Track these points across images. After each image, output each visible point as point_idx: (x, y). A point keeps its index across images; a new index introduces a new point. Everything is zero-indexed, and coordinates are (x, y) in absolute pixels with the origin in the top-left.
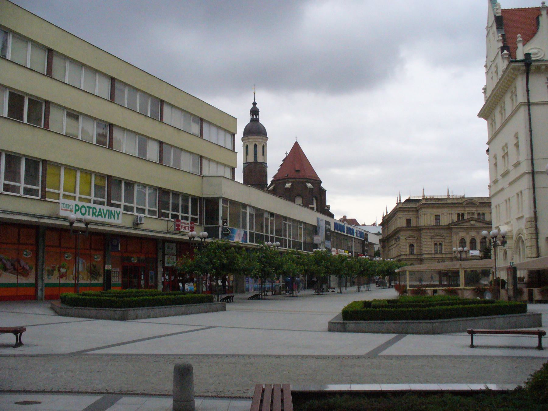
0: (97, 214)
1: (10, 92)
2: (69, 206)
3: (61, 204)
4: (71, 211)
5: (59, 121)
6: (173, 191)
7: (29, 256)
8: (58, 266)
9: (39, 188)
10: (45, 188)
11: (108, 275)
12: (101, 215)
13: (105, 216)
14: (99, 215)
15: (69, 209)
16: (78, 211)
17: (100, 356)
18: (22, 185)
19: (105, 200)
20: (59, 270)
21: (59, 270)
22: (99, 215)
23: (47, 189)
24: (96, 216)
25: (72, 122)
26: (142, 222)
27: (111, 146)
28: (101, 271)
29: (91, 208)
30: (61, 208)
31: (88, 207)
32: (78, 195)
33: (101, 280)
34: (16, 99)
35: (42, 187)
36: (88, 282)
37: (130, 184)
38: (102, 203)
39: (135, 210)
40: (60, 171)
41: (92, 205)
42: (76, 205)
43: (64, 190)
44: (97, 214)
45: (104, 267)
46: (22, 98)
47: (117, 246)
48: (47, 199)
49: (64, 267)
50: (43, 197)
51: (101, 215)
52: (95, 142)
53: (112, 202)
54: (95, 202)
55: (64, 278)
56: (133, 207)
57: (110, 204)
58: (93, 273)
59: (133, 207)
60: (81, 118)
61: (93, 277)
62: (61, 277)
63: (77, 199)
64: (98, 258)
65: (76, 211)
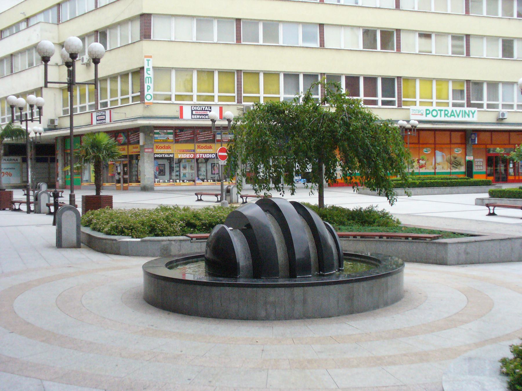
0: (449, 115)
1: (263, 23)
2: (419, 111)
3: (411, 110)
4: (422, 115)
5: (410, 43)
6: (130, 70)
7: (460, 152)
8: (417, 159)
9: (396, 99)
10: (470, 101)
11: (469, 165)
12: (454, 115)
13: (458, 116)
14: (451, 115)
15: (420, 113)
16: (429, 114)
17: (111, 241)
18: (380, 98)
19: (465, 101)
20: (418, 162)
21: (418, 162)
22: (451, 115)
23: (403, 99)
24: (448, 117)
25: (424, 40)
26: (505, 117)
27: (468, 54)
28: (463, 162)
29: (442, 110)
30: (411, 113)
31: (439, 110)
32: (418, 100)
33: (463, 169)
34: (369, 34)
35: (398, 98)
36: (449, 171)
37: (493, 85)
38: (461, 105)
39: (500, 106)
40: (415, 84)
41: (434, 107)
42: (427, 110)
43: (219, 92)
44: (449, 115)
45: (465, 158)
46: (374, 32)
47: (475, 139)
48: (403, 107)
49: (423, 160)
50: (400, 105)
51: (454, 115)
52: (450, 54)
53: (472, 102)
54: (454, 105)
55: (424, 168)
56: (498, 105)
57: (469, 105)
58: (455, 163)
59: (498, 105)
60: (433, 36)
61: (453, 166)
62: (421, 167)
63: (434, 104)
64: (458, 151)
65: (427, 114)
